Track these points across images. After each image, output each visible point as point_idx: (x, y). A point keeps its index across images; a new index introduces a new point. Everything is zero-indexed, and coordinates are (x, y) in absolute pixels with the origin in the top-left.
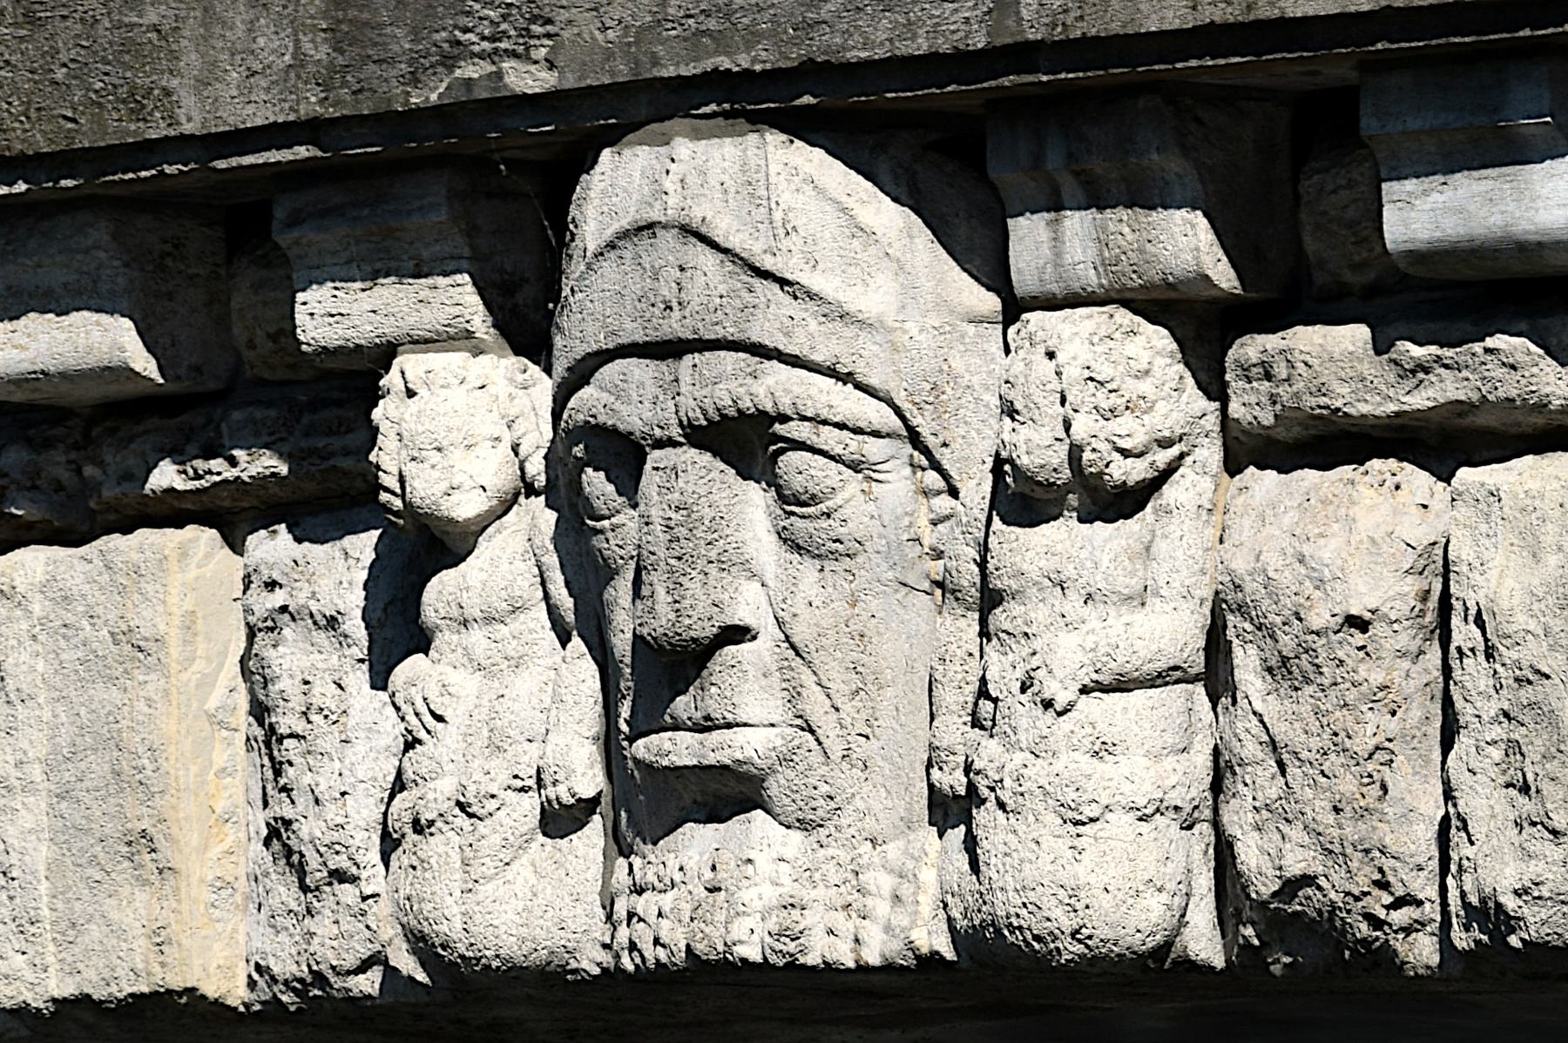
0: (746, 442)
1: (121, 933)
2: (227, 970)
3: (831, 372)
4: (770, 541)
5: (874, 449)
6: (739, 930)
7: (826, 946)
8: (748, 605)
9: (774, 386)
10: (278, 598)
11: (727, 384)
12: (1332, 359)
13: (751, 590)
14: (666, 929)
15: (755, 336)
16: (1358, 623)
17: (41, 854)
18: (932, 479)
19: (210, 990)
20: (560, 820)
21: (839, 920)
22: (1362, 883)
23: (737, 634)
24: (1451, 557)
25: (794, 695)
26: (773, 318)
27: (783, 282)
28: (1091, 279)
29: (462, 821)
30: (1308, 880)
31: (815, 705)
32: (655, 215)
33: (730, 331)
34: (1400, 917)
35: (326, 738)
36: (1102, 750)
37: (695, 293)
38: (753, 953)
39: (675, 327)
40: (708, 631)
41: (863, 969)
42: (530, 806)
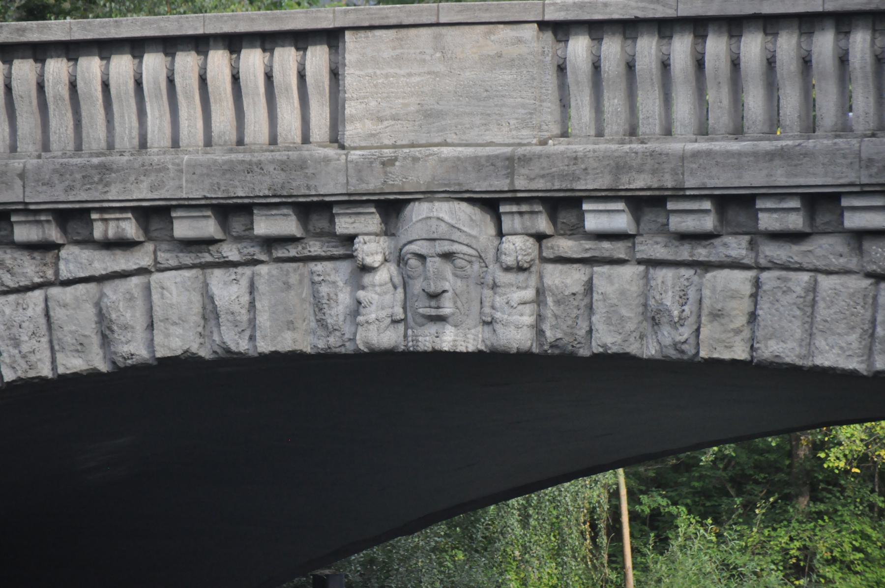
0: (448, 256)
1: (285, 339)
2: (307, 346)
3: (467, 245)
4: (450, 275)
5: (474, 259)
6: (444, 345)
7: (462, 348)
8: (447, 286)
9: (456, 247)
10: (322, 278)
11: (446, 247)
12: (566, 246)
13: (447, 284)
14: (427, 343)
15: (453, 238)
16: (574, 294)
17: (268, 324)
18: (483, 265)
19: (305, 350)
20: (395, 322)
21: (462, 343)
22: (571, 340)
23: (444, 291)
24: (437, 242)
25: (455, 303)
26: (456, 236)
27: (458, 229)
28: (519, 230)
29: (377, 322)
30: (561, 339)
31: (459, 304)
32: (431, 215)
33: (447, 237)
34: (578, 346)
35: (333, 304)
36: (521, 315)
37: (440, 230)
38: (446, 349)
39: (435, 236)
40: (440, 291)
41: (468, 353)
42: (389, 320)
